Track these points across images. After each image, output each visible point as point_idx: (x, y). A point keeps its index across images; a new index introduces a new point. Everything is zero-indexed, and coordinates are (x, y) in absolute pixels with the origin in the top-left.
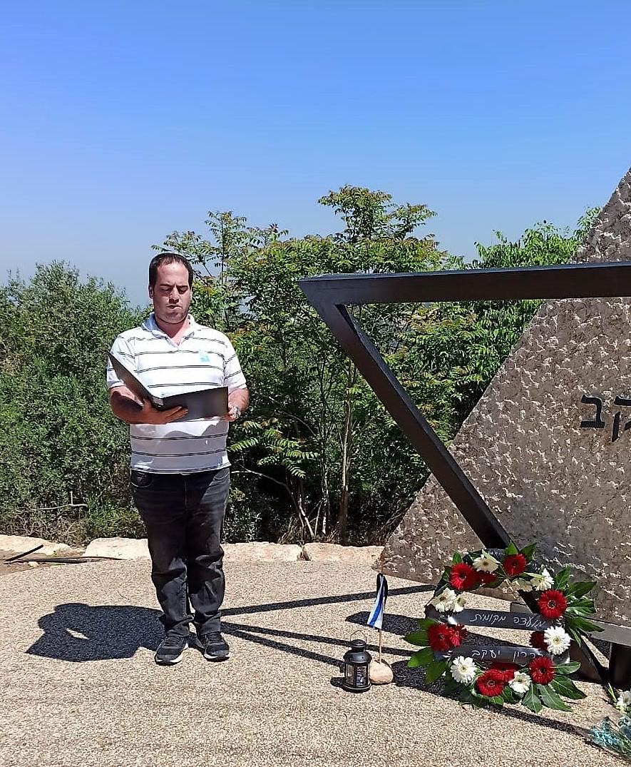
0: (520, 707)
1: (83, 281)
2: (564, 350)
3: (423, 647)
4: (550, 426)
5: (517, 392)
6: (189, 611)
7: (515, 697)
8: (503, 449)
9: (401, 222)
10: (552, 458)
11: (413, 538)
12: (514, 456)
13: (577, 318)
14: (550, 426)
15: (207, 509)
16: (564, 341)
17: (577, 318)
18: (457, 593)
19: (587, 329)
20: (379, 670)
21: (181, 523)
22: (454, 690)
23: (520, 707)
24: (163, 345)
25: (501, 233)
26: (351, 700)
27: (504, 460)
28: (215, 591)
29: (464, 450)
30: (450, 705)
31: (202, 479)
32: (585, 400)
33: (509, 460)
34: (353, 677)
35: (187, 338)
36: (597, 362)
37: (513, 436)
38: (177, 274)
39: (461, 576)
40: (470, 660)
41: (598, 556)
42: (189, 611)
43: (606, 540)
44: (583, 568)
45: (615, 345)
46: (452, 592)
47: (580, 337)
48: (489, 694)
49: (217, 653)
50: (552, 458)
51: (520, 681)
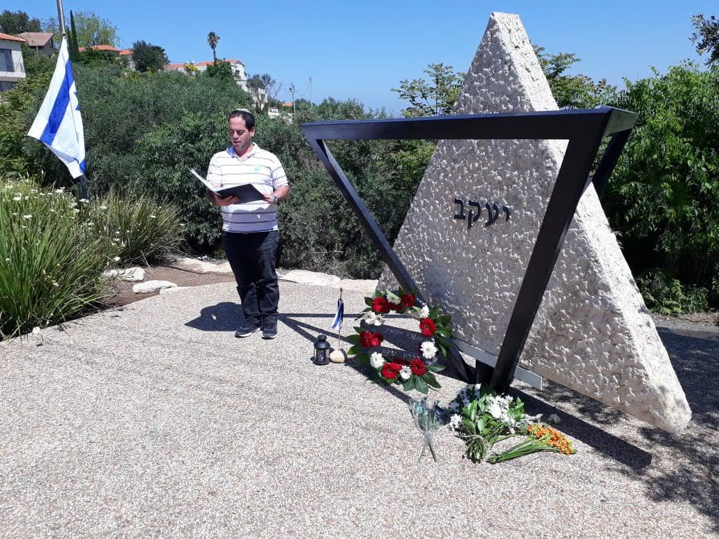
0: (400, 388)
1: (366, 111)
2: (448, 169)
3: (396, 348)
4: (443, 217)
5: (428, 195)
6: (256, 309)
7: (401, 380)
8: (424, 230)
9: (554, 66)
10: (444, 238)
11: (388, 281)
12: (428, 234)
13: (454, 148)
14: (443, 217)
15: (260, 253)
16: (449, 163)
17: (454, 148)
18: (376, 314)
19: (458, 156)
20: (337, 355)
21: (255, 263)
22: (370, 373)
23: (400, 388)
24: (235, 161)
25: (656, 68)
26: (320, 369)
27: (424, 237)
28: (272, 300)
29: (407, 229)
30: (359, 377)
31: (261, 237)
32: (457, 201)
33: (426, 237)
34: (321, 358)
35: (249, 157)
36: (463, 177)
37: (427, 222)
38: (240, 124)
39: (380, 305)
40: (380, 355)
41: (465, 301)
42: (256, 309)
43: (468, 292)
44: (457, 308)
45: (471, 166)
46: (374, 313)
47: (455, 161)
48: (383, 378)
49: (269, 331)
50: (444, 238)
51: (406, 372)
